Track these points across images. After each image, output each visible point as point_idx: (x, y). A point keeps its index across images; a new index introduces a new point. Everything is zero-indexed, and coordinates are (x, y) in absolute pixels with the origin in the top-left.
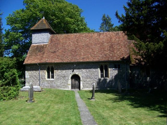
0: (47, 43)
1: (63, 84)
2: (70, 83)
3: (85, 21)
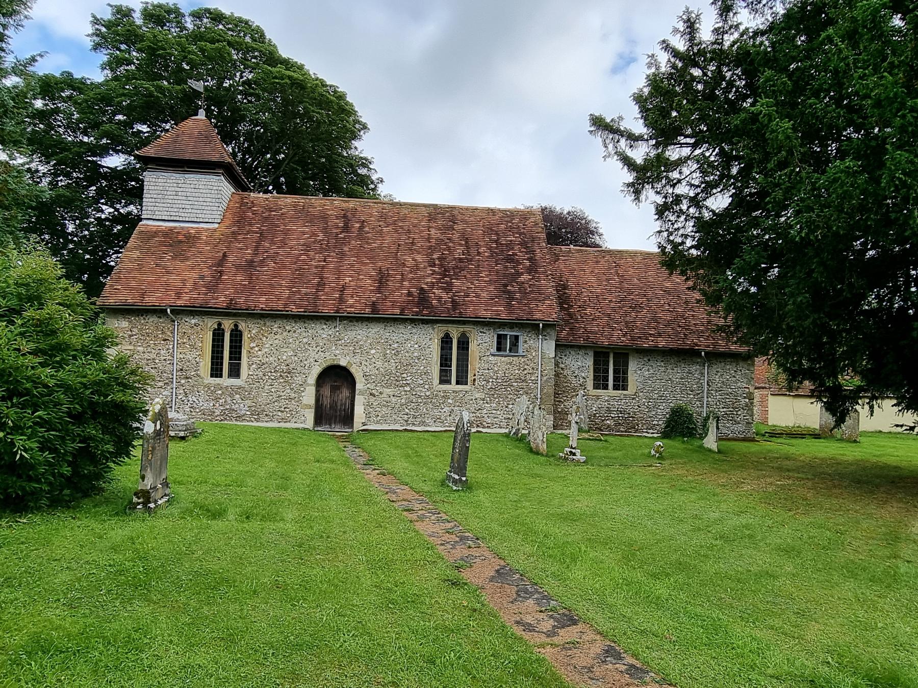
0: (216, 226)
1: (283, 403)
2: (312, 401)
3: (90, 31)
